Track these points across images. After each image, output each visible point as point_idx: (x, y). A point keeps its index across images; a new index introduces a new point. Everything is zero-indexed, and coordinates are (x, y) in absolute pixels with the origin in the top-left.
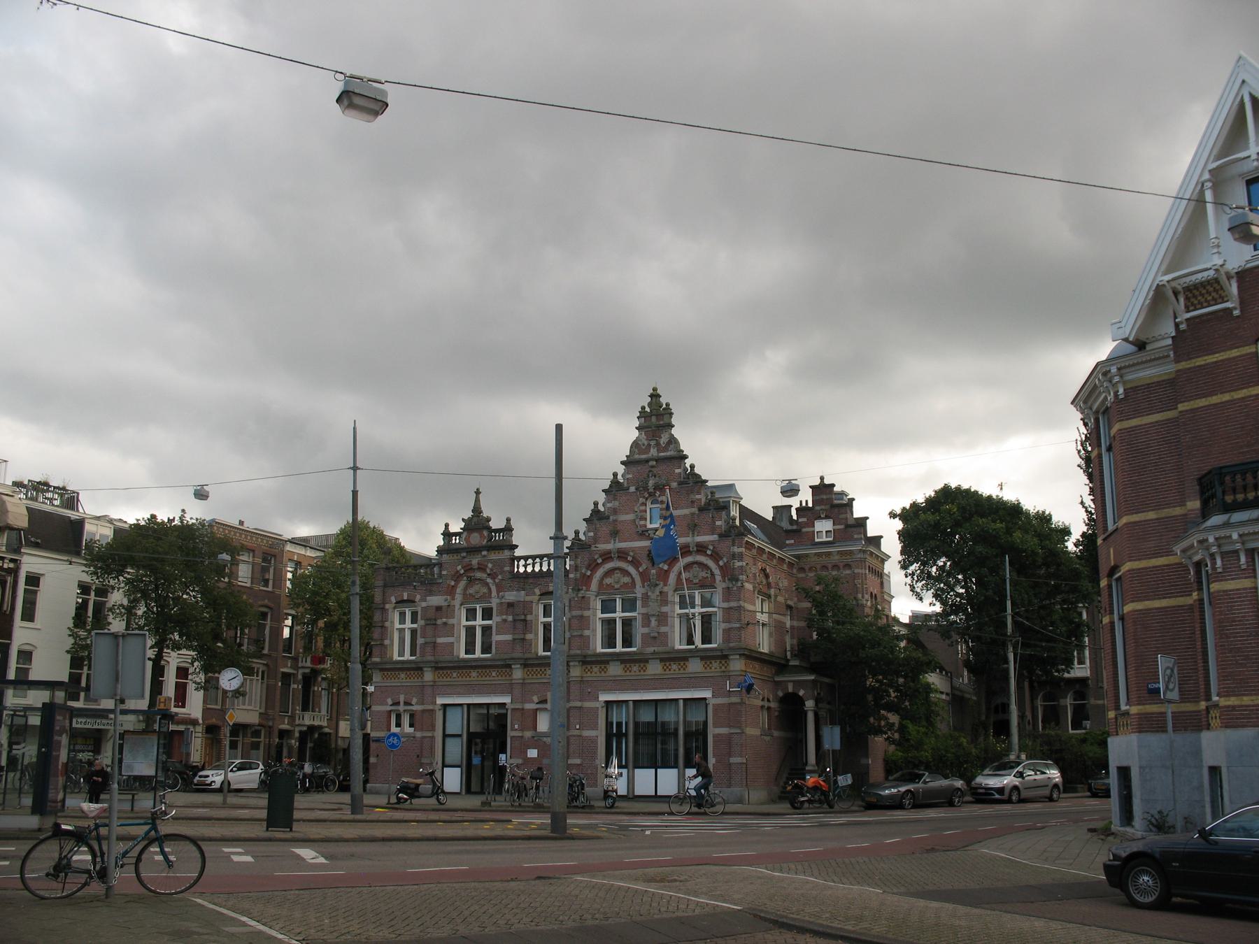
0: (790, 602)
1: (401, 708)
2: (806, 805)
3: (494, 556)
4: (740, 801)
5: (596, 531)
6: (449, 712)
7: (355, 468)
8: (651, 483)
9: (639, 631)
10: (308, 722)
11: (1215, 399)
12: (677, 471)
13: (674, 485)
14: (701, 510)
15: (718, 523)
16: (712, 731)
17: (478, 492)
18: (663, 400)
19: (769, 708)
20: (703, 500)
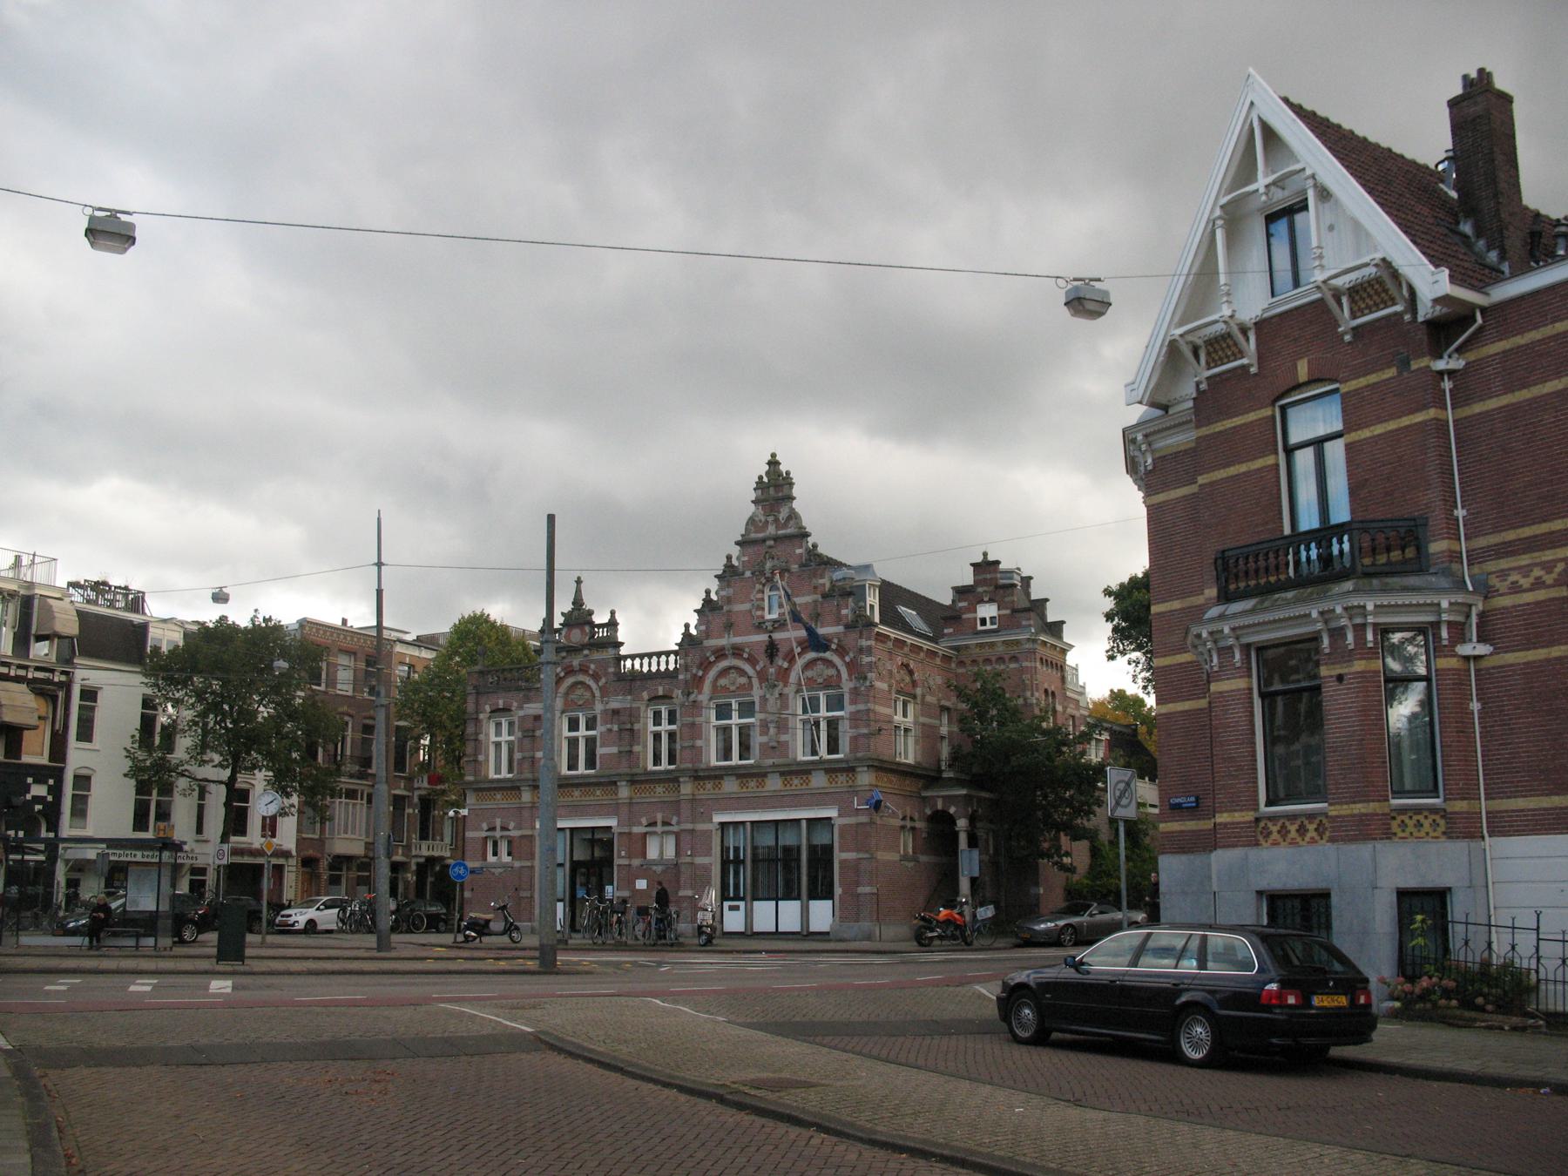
0: (943, 703)
1: (498, 834)
2: (937, 942)
3: (597, 656)
4: (869, 938)
5: (708, 623)
7: (379, 564)
8: (769, 565)
9: (757, 740)
10: (425, 853)
11: (1232, 471)
12: (798, 551)
13: (795, 567)
14: (825, 596)
15: (844, 612)
16: (839, 856)
17: (579, 582)
18: (783, 468)
19: (913, 829)
20: (828, 586)
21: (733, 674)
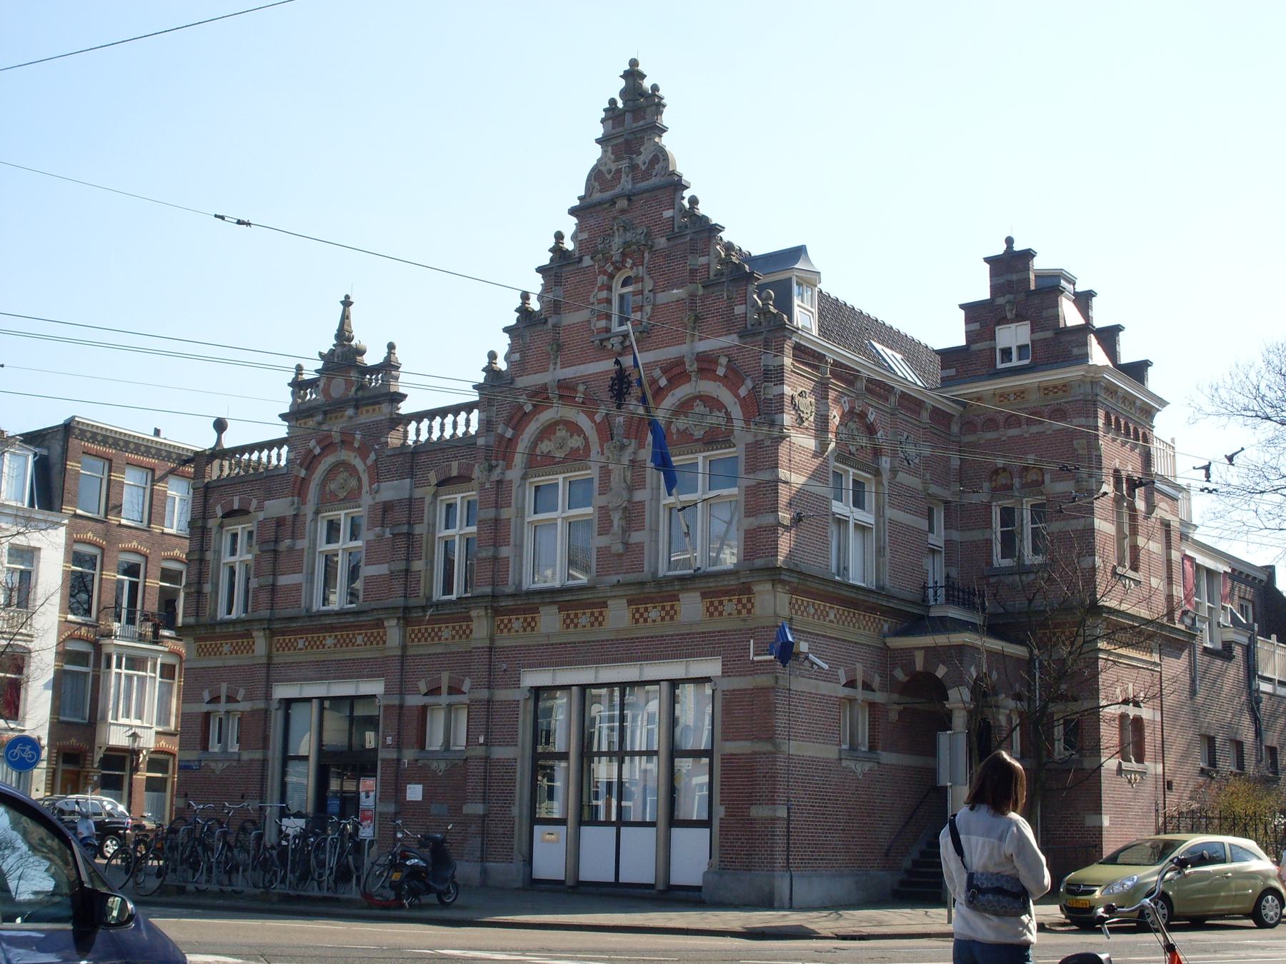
6: (297, 712)
12: (668, 214)
17: (347, 303)
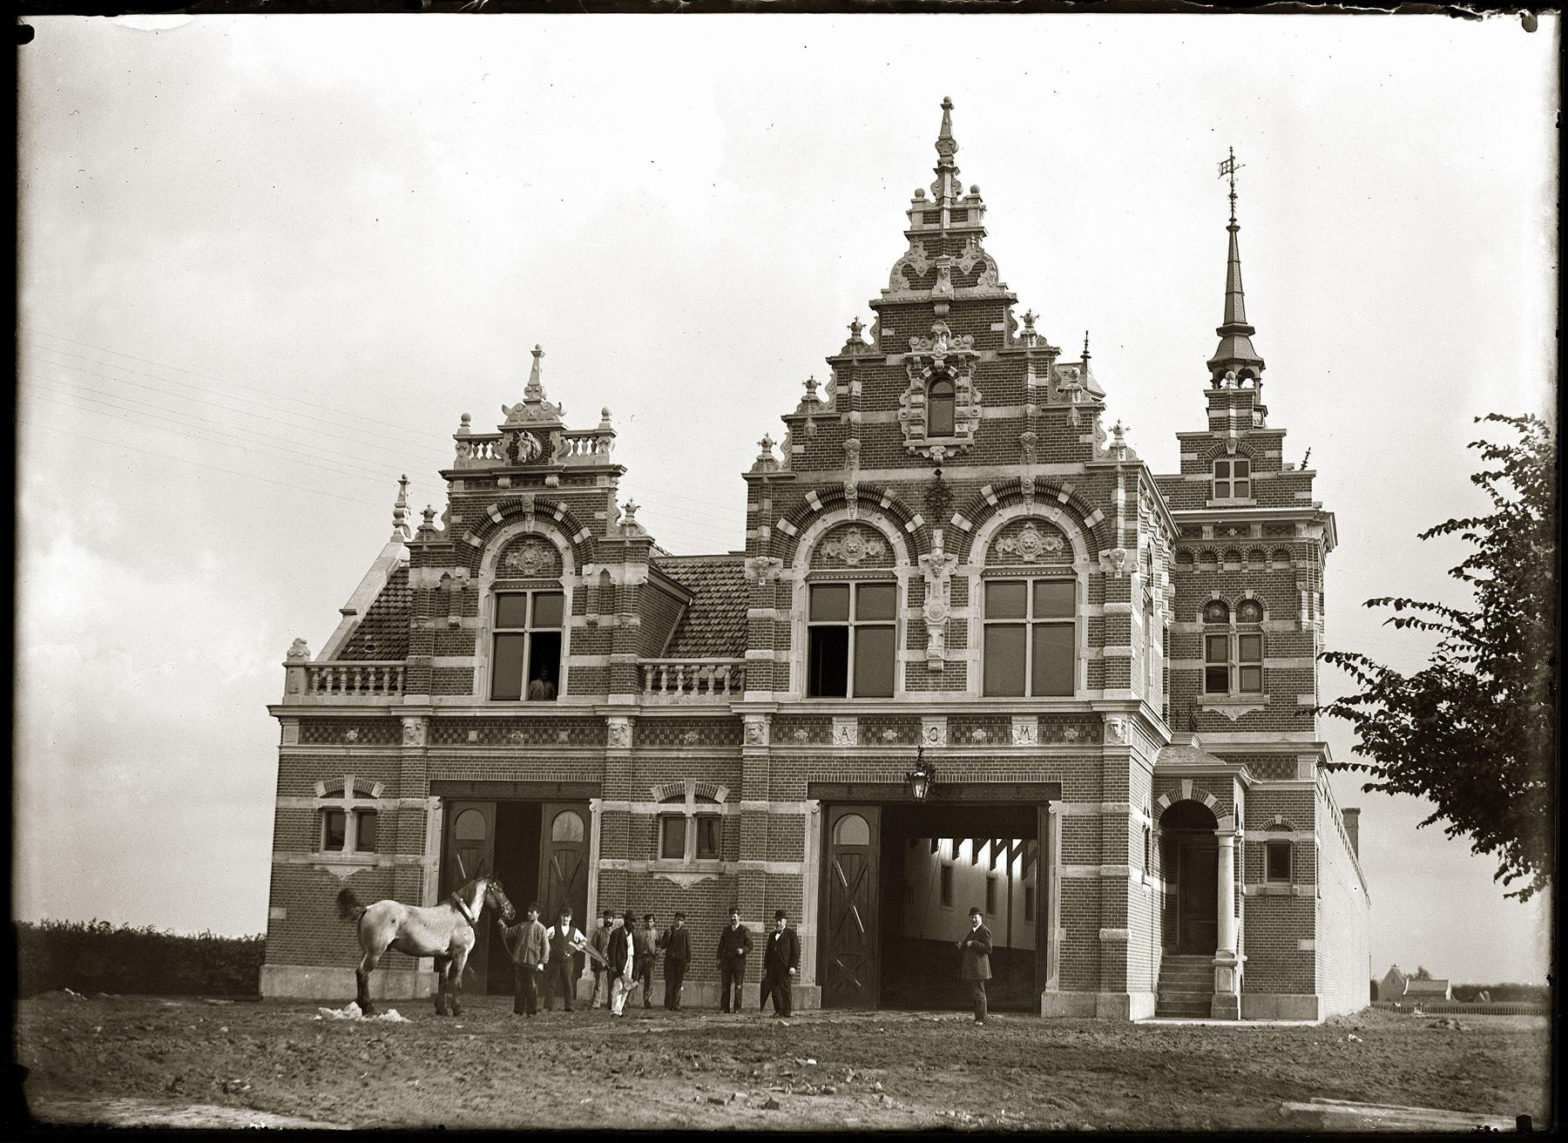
21: (1030, 536)
